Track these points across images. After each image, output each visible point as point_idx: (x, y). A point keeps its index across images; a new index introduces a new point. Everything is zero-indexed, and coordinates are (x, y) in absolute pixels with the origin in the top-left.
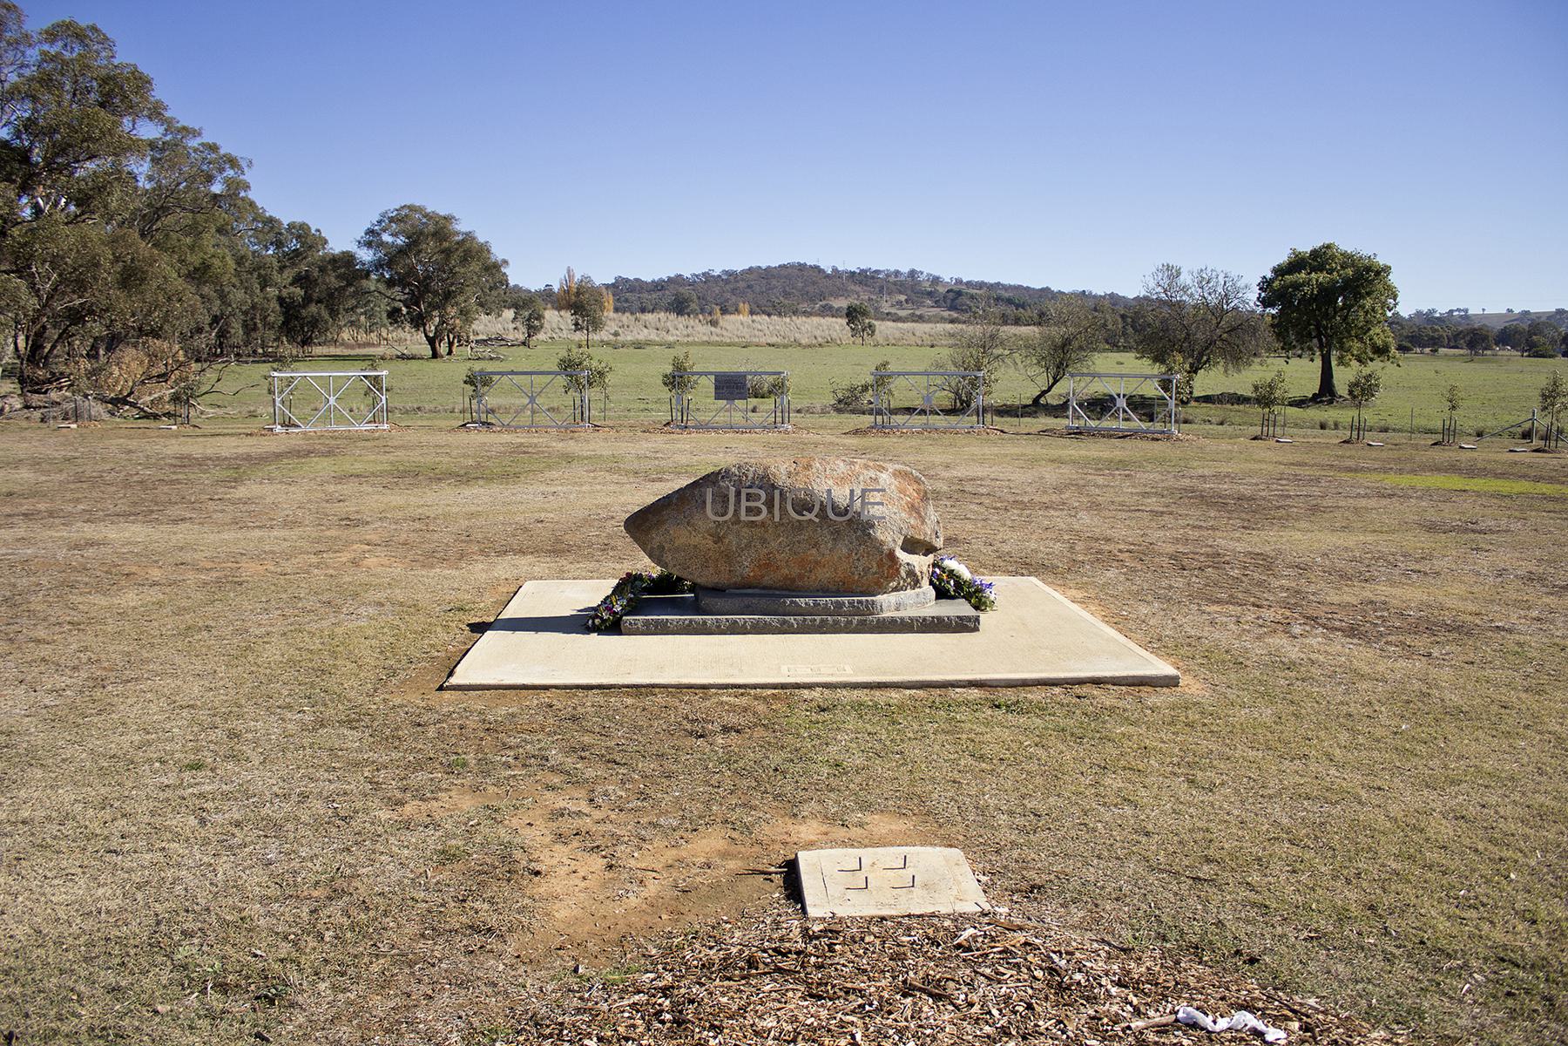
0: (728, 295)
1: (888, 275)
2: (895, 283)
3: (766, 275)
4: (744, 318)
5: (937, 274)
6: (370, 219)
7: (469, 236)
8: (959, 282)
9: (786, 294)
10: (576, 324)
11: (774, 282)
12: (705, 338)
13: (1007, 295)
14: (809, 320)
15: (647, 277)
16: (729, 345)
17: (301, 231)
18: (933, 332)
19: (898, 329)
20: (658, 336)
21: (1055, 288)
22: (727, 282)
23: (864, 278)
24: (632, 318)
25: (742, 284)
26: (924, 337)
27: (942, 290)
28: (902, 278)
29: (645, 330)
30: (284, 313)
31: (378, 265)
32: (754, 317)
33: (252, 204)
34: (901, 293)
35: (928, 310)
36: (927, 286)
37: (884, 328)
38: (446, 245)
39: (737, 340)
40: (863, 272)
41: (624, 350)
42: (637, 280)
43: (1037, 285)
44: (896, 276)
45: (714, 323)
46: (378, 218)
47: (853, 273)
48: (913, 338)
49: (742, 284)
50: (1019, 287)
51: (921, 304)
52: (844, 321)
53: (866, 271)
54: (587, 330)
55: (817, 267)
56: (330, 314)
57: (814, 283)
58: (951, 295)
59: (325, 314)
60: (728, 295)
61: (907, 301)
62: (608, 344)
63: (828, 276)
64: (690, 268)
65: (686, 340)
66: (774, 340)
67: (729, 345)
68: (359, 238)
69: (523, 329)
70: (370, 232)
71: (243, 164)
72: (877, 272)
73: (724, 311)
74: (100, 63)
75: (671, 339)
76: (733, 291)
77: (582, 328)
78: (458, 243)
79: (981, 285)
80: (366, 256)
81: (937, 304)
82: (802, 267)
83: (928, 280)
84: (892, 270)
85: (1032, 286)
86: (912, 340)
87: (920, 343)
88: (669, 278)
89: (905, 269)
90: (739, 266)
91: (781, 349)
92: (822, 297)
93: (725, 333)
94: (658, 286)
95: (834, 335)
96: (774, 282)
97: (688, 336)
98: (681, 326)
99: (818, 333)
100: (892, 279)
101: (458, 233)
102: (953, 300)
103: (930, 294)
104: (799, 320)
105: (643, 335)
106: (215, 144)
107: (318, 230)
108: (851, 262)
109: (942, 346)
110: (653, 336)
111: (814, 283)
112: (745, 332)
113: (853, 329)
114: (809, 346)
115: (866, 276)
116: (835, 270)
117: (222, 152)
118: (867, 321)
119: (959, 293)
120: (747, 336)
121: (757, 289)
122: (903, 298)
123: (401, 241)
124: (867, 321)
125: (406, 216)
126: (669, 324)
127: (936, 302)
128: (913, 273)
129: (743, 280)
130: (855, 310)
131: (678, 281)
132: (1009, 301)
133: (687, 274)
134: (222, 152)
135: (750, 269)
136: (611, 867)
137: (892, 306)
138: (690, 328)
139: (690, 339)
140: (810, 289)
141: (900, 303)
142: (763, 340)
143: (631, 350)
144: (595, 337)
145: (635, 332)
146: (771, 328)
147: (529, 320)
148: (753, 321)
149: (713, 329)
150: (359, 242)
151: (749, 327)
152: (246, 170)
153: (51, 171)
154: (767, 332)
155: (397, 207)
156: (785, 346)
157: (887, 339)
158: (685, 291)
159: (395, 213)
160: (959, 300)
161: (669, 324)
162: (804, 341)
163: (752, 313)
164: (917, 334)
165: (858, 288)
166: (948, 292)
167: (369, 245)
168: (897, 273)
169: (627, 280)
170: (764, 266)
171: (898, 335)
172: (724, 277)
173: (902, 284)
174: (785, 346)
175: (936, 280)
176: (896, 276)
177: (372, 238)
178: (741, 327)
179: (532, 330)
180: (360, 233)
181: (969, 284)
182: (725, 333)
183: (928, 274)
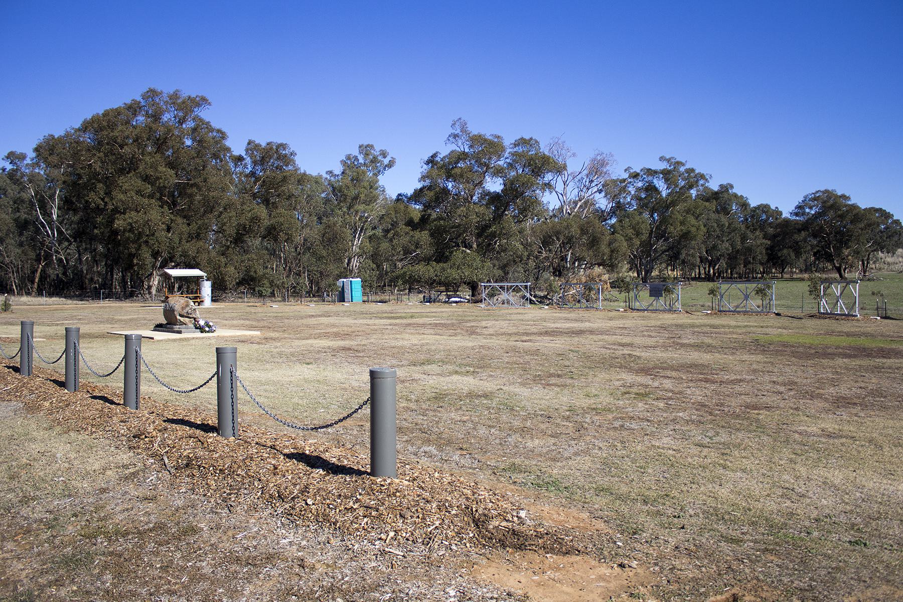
6: (798, 199)
68: (791, 211)
70: (798, 207)
107: (777, 208)
117: (697, 172)
134: (697, 172)
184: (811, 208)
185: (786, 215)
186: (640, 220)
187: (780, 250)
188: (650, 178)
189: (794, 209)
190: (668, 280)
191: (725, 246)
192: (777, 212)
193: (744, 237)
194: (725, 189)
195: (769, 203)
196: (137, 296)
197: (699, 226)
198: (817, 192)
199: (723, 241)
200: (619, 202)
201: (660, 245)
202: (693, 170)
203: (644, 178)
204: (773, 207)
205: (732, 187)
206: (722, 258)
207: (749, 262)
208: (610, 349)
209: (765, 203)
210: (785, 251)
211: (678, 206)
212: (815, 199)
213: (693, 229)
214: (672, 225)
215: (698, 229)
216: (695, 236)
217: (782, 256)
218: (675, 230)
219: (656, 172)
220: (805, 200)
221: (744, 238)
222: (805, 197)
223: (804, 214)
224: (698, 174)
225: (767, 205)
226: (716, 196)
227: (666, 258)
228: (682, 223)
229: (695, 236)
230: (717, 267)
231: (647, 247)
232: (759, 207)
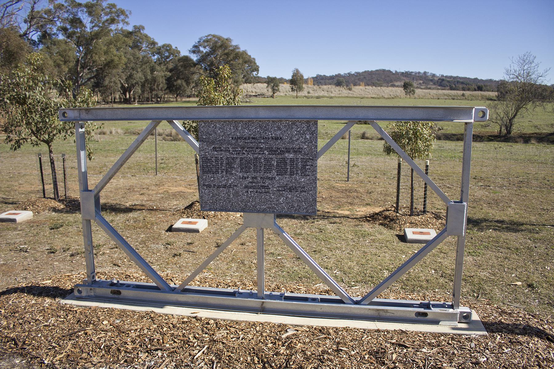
0: (357, 81)
1: (416, 74)
2: (418, 76)
4: (362, 87)
6: (194, 41)
7: (237, 47)
8: (442, 76)
9: (378, 80)
10: (292, 89)
11: (374, 76)
12: (346, 95)
13: (461, 81)
15: (328, 75)
16: (356, 98)
17: (167, 47)
18: (437, 93)
19: (423, 92)
20: (328, 94)
21: (479, 78)
22: (356, 76)
23: (407, 74)
24: (318, 87)
25: (362, 77)
26: (434, 95)
27: (436, 79)
28: (421, 75)
29: (323, 92)
30: (167, 84)
31: (199, 62)
32: (366, 87)
33: (146, 36)
34: (421, 80)
35: (431, 85)
36: (430, 78)
37: (418, 91)
38: (226, 51)
39: (359, 96)
40: (406, 72)
41: (312, 99)
42: (324, 76)
43: (472, 77)
44: (419, 74)
45: (350, 89)
46: (198, 40)
47: (403, 73)
48: (429, 96)
49: (362, 77)
50: (466, 78)
51: (429, 84)
52: (402, 89)
54: (297, 91)
56: (186, 84)
57: (388, 76)
58: (440, 81)
59: (184, 84)
60: (357, 81)
61: (423, 83)
62: (306, 96)
63: (393, 74)
64: (343, 71)
65: (338, 96)
66: (374, 96)
67: (356, 98)
68: (190, 49)
69: (270, 90)
70: (195, 46)
71: (127, 13)
72: (412, 72)
73: (355, 85)
75: (332, 95)
76: (359, 79)
77: (295, 90)
78: (232, 50)
79: (451, 77)
80: (194, 58)
81: (434, 84)
82: (384, 71)
85: (470, 77)
86: (429, 97)
87: (432, 97)
88: (336, 75)
89: (422, 71)
90: (361, 70)
91: (377, 99)
92: (391, 81)
93: (354, 93)
94: (332, 78)
95: (398, 94)
96: (374, 76)
97: (340, 94)
98: (337, 90)
99: (391, 93)
100: (417, 75)
101: (231, 46)
102: (441, 83)
103: (431, 80)
104: (383, 88)
105: (322, 94)
106: (114, 4)
107: (176, 47)
108: (402, 69)
109: (441, 99)
110: (326, 94)
111: (388, 76)
112: (362, 93)
113: (406, 92)
114: (388, 98)
115: (408, 74)
116: (396, 72)
117: (118, 7)
118: (412, 89)
119: (443, 80)
120: (363, 94)
121: (368, 78)
122: (421, 82)
123: (208, 49)
124: (412, 89)
125: (210, 39)
126: (332, 89)
127: (434, 83)
128: (425, 73)
129: (362, 75)
130: (407, 84)
131: (339, 76)
132: (462, 83)
133: (342, 73)
134: (118, 7)
137: (418, 85)
139: (340, 95)
140: (387, 79)
141: (420, 84)
142: (369, 96)
143: (315, 99)
144: (300, 94)
145: (319, 93)
146: (373, 91)
147: (273, 87)
148: (366, 89)
149: (350, 92)
150: (190, 51)
151: (364, 91)
152: (129, 15)
154: (371, 93)
155: (206, 35)
156: (378, 98)
157: (419, 96)
158: (341, 79)
159: (206, 38)
160: (444, 82)
161: (332, 89)
162: (386, 96)
163: (365, 86)
164: (431, 94)
166: (439, 79)
167: (194, 52)
168: (419, 73)
169: (321, 76)
170: (370, 70)
171: (423, 94)
173: (421, 77)
174: (378, 98)
175: (434, 75)
176: (419, 74)
177: (195, 49)
178: (361, 91)
179: (274, 91)
180: (190, 47)
181: (446, 77)
182: (354, 93)
183: (431, 73)
184: (205, 47)
185: (184, 53)
186: (67, 48)
187: (175, 81)
188: (75, 10)
189: (192, 47)
190: (476, 88)
191: (139, 76)
192: (177, 51)
193: (153, 69)
194: (138, 29)
195: (171, 43)
196: (343, 86)
197: (121, 56)
198: (209, 35)
199: (138, 72)
200: (46, 32)
201: (85, 74)
202: (114, 6)
203: (69, 9)
204: (174, 47)
205: (143, 28)
206: (137, 85)
207: (154, 90)
208: (530, 232)
209: (168, 43)
210: (179, 82)
211: (100, 39)
212: (207, 41)
213: (116, 59)
214: (96, 54)
215: (119, 59)
216: (117, 65)
217: (177, 85)
218: (102, 59)
219: (80, 5)
220: (200, 41)
221: (152, 70)
222: (200, 39)
223: (199, 51)
224: (119, 9)
225: (169, 44)
226: (129, 34)
227: (91, 85)
228: (106, 53)
229: (117, 65)
230: (132, 93)
231: (74, 75)
232: (163, 46)
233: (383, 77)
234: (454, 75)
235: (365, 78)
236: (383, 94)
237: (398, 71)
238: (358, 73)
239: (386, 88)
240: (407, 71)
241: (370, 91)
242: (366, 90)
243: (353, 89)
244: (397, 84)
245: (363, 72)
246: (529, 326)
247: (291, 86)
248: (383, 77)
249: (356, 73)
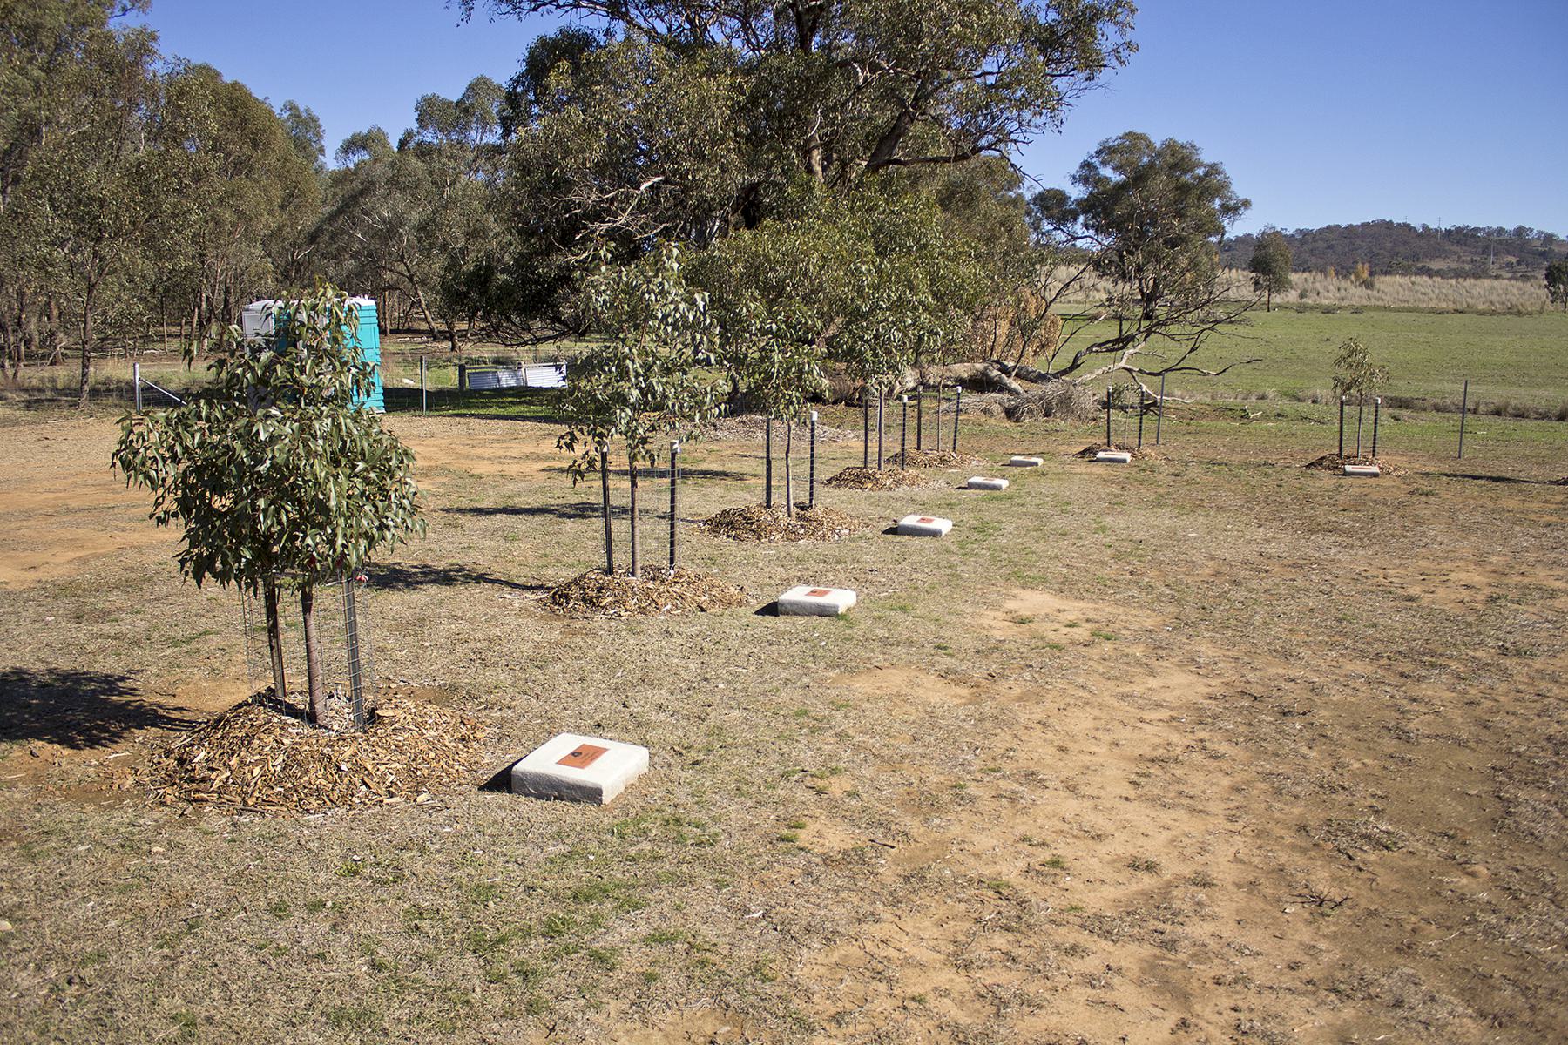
3: (1350, 234)
5: (1549, 231)
6: (1086, 148)
11: (1358, 242)
14: (1479, 282)
25: (1321, 245)
28: (1506, 237)
34: (1509, 253)
40: (1459, 230)
49: (1321, 245)
53: (1463, 229)
55: (1406, 225)
57: (1405, 243)
60: (1306, 256)
61: (1519, 263)
63: (1420, 235)
68: (1073, 172)
70: (1087, 165)
72: (1477, 230)
74: (1090, 912)
83: (1539, 239)
84: (1495, 227)
89: (1510, 226)
90: (1315, 225)
92: (1416, 257)
99: (1494, 298)
100: (1495, 237)
108: (1443, 219)
111: (1405, 243)
113: (1552, 294)
116: (1425, 228)
126: (1318, 285)
128: (1520, 231)
129: (1322, 239)
135: (1329, 227)
136: (1350, 805)
138: (1342, 291)
144: (1277, 299)
149: (1369, 292)
150: (1074, 177)
153: (945, 353)
161: (1318, 285)
165: (1455, 248)
167: (1085, 180)
168: (1500, 231)
172: (1298, 237)
177: (1087, 173)
178: (1401, 290)
180: (1074, 168)
183: (1539, 232)
233: (1389, 245)
234: (1369, 219)
235: (1330, 247)
236: (1470, 300)
237: (1432, 226)
238: (1305, 234)
239: (1472, 281)
240: (1460, 224)
241: (1429, 290)
242: (1416, 288)
243: (1377, 285)
244: (1436, 265)
245: (1321, 231)
246: (987, 375)
247: (1253, 275)
248: (1389, 245)
249: (1299, 231)
